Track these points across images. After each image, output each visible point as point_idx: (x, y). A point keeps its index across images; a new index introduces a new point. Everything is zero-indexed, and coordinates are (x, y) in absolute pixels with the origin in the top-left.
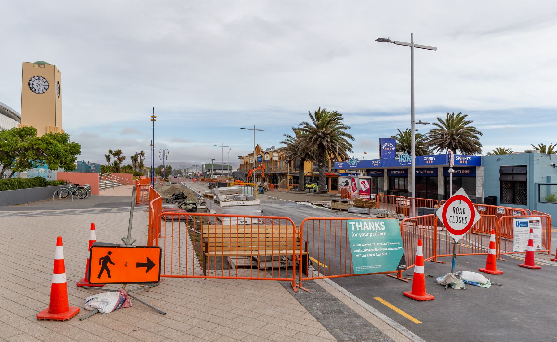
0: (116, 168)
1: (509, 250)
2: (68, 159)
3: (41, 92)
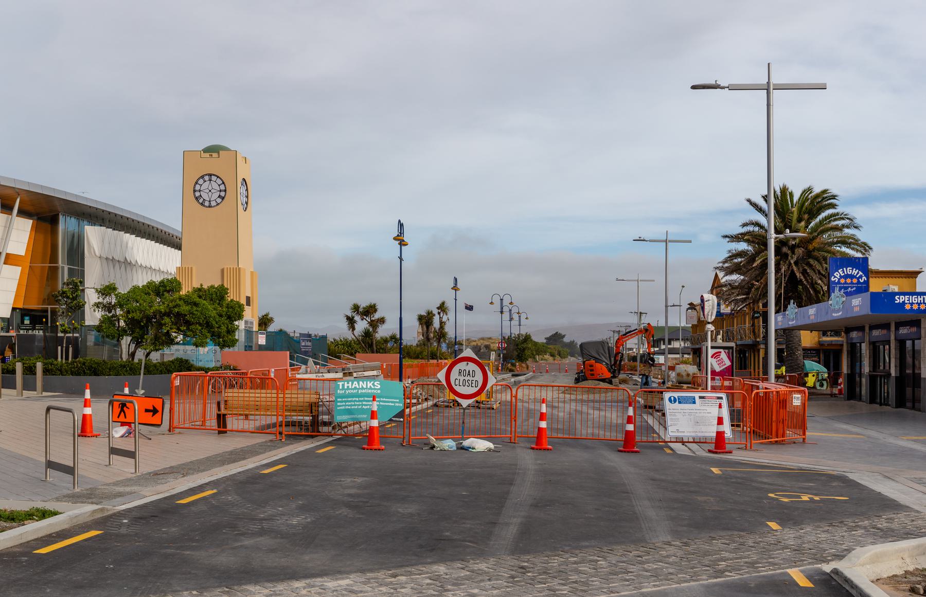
0: (368, 344)
2: (224, 328)
3: (213, 204)
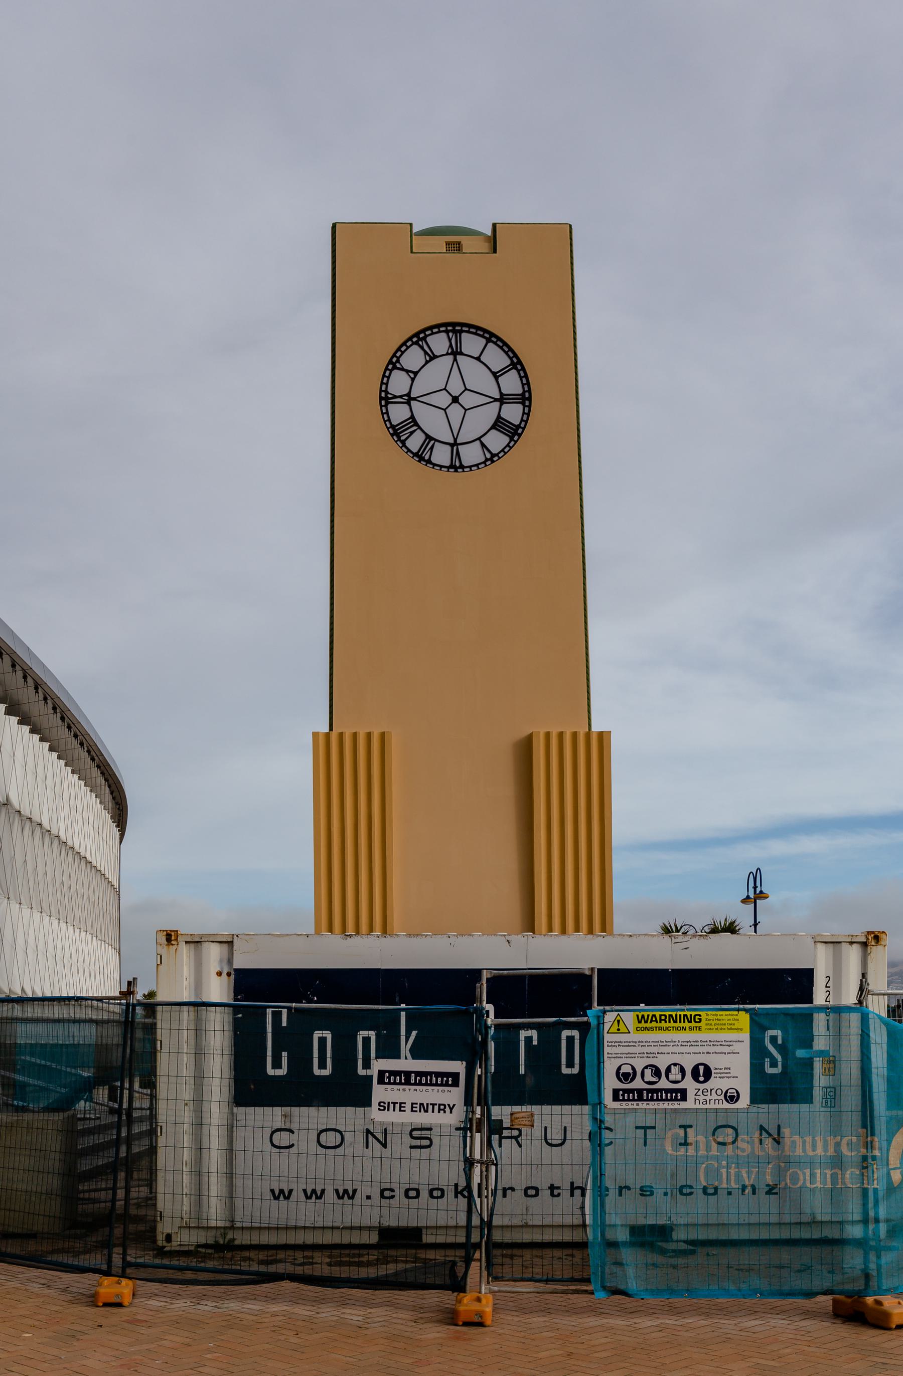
1: (708, 1027)
3: (471, 454)
